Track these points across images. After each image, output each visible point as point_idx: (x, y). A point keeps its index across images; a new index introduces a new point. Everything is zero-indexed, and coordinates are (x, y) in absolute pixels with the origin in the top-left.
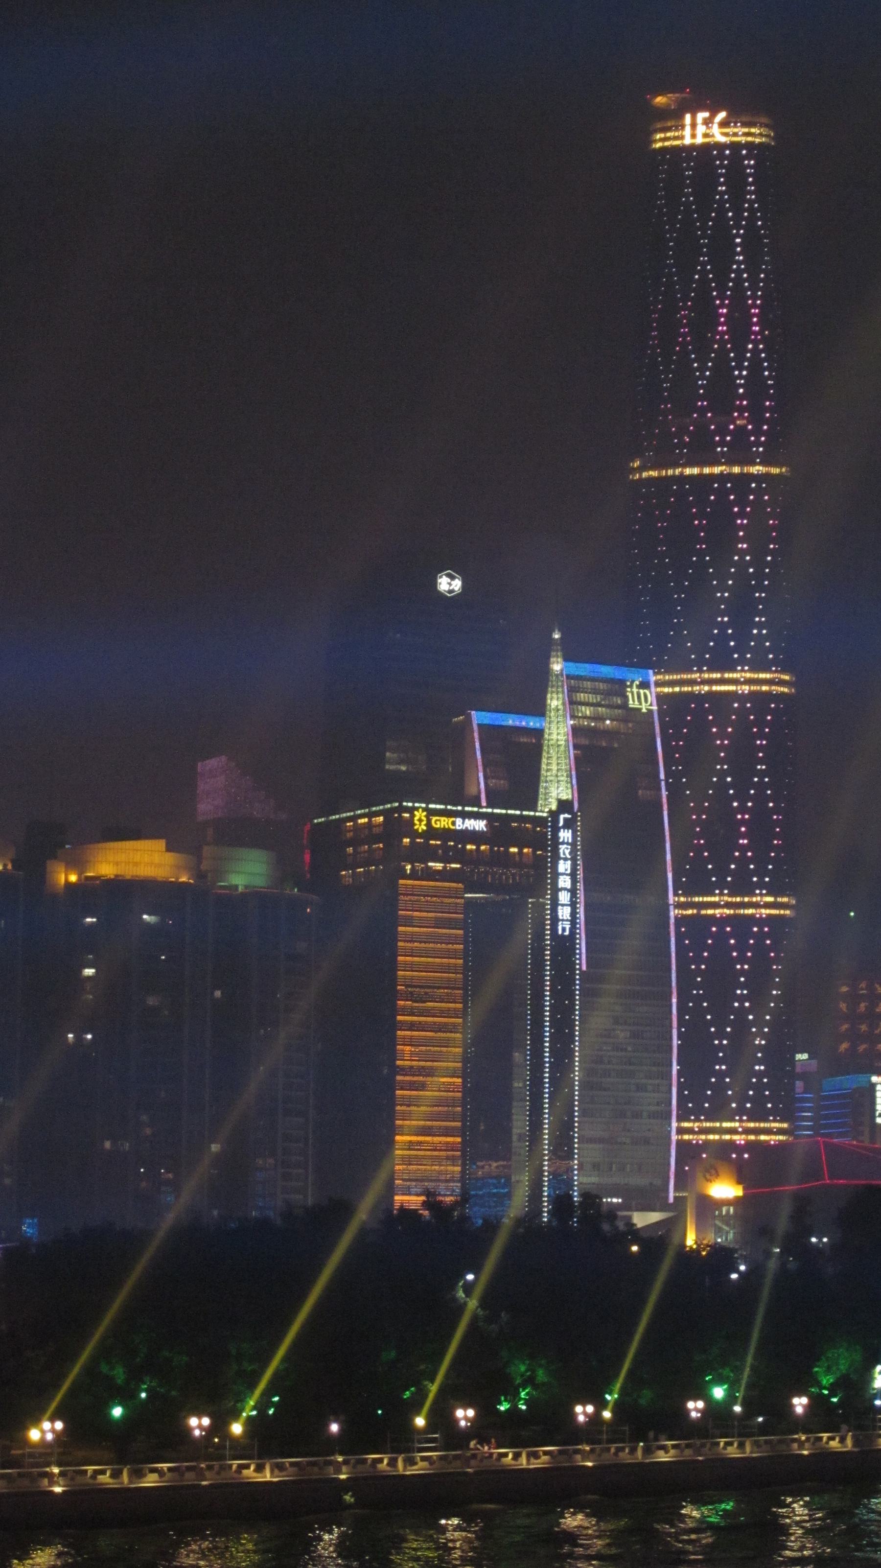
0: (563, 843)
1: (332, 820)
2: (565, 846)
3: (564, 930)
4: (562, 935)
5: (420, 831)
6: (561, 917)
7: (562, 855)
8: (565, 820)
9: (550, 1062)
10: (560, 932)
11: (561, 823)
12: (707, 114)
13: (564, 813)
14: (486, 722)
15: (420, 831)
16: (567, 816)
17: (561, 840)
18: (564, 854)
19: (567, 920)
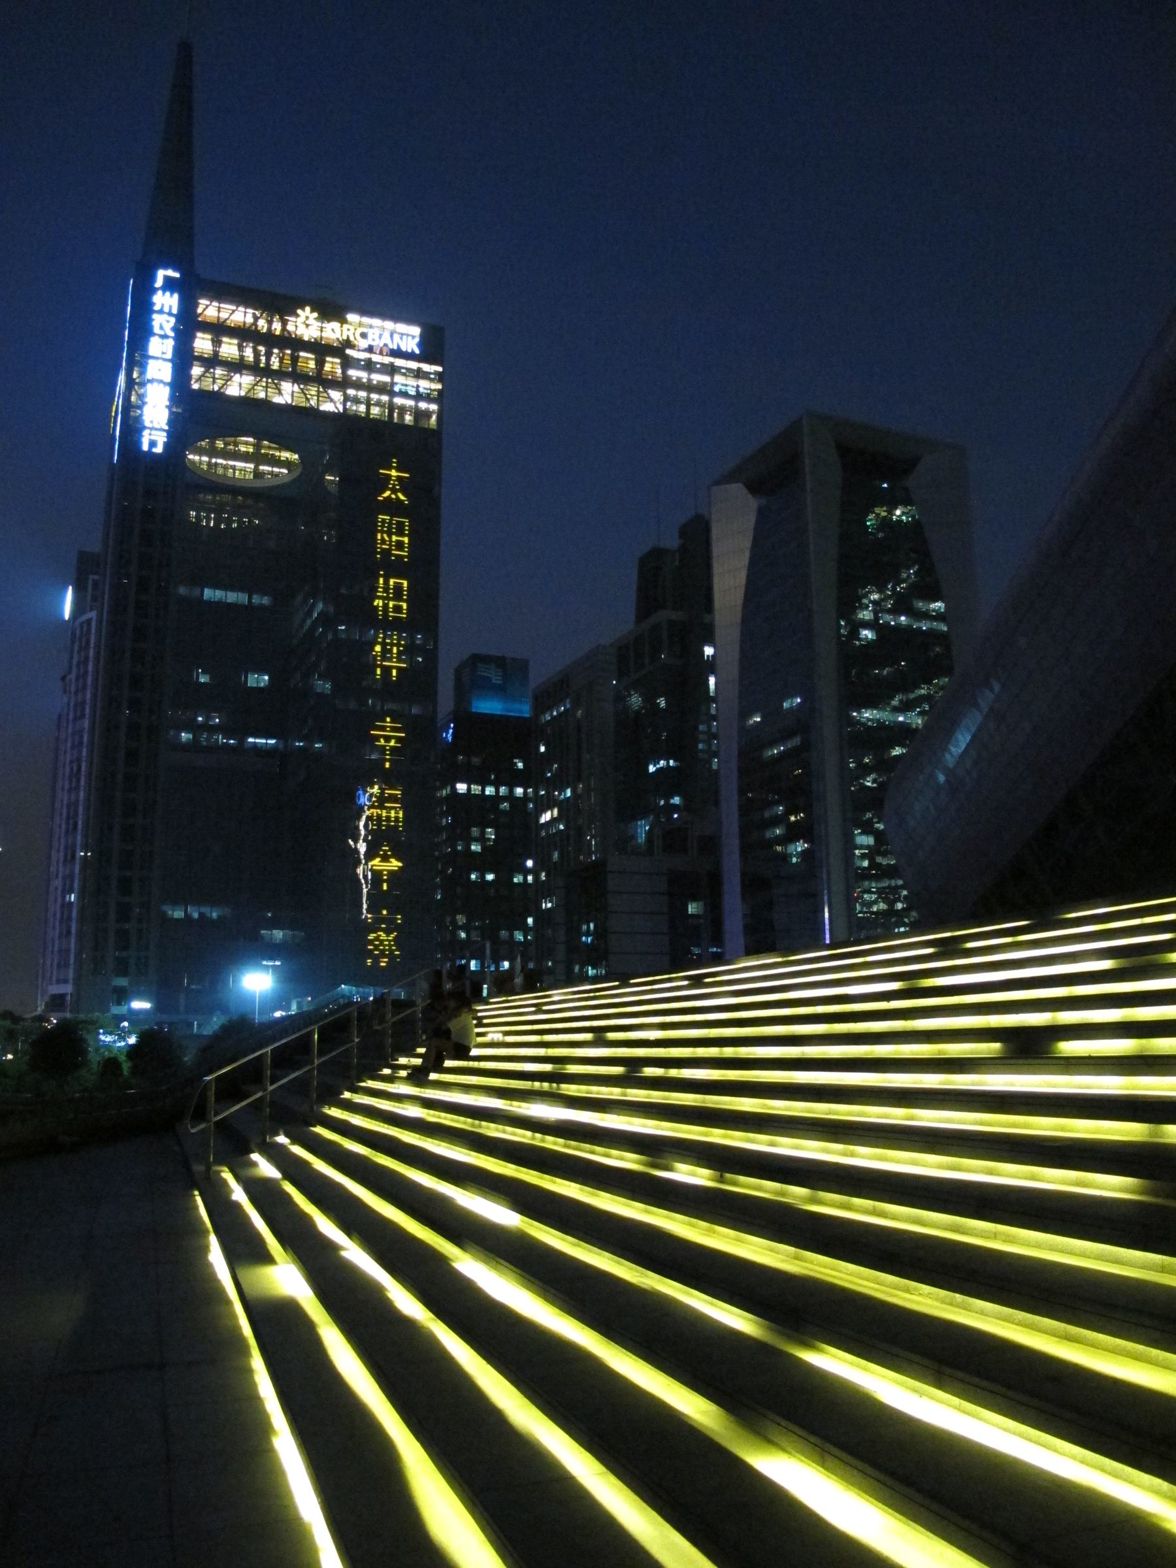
0: (161, 312)
1: (241, 589)
2: (165, 317)
3: (153, 444)
4: (150, 452)
5: (308, 309)
6: (147, 424)
7: (156, 330)
8: (167, 279)
9: (497, 798)
10: (145, 447)
11: (159, 283)
12: (154, 450)
13: (166, 267)
14: (741, 941)
15: (308, 309)
16: (96, 577)
17: (156, 308)
18: (161, 328)
19: (162, 430)
